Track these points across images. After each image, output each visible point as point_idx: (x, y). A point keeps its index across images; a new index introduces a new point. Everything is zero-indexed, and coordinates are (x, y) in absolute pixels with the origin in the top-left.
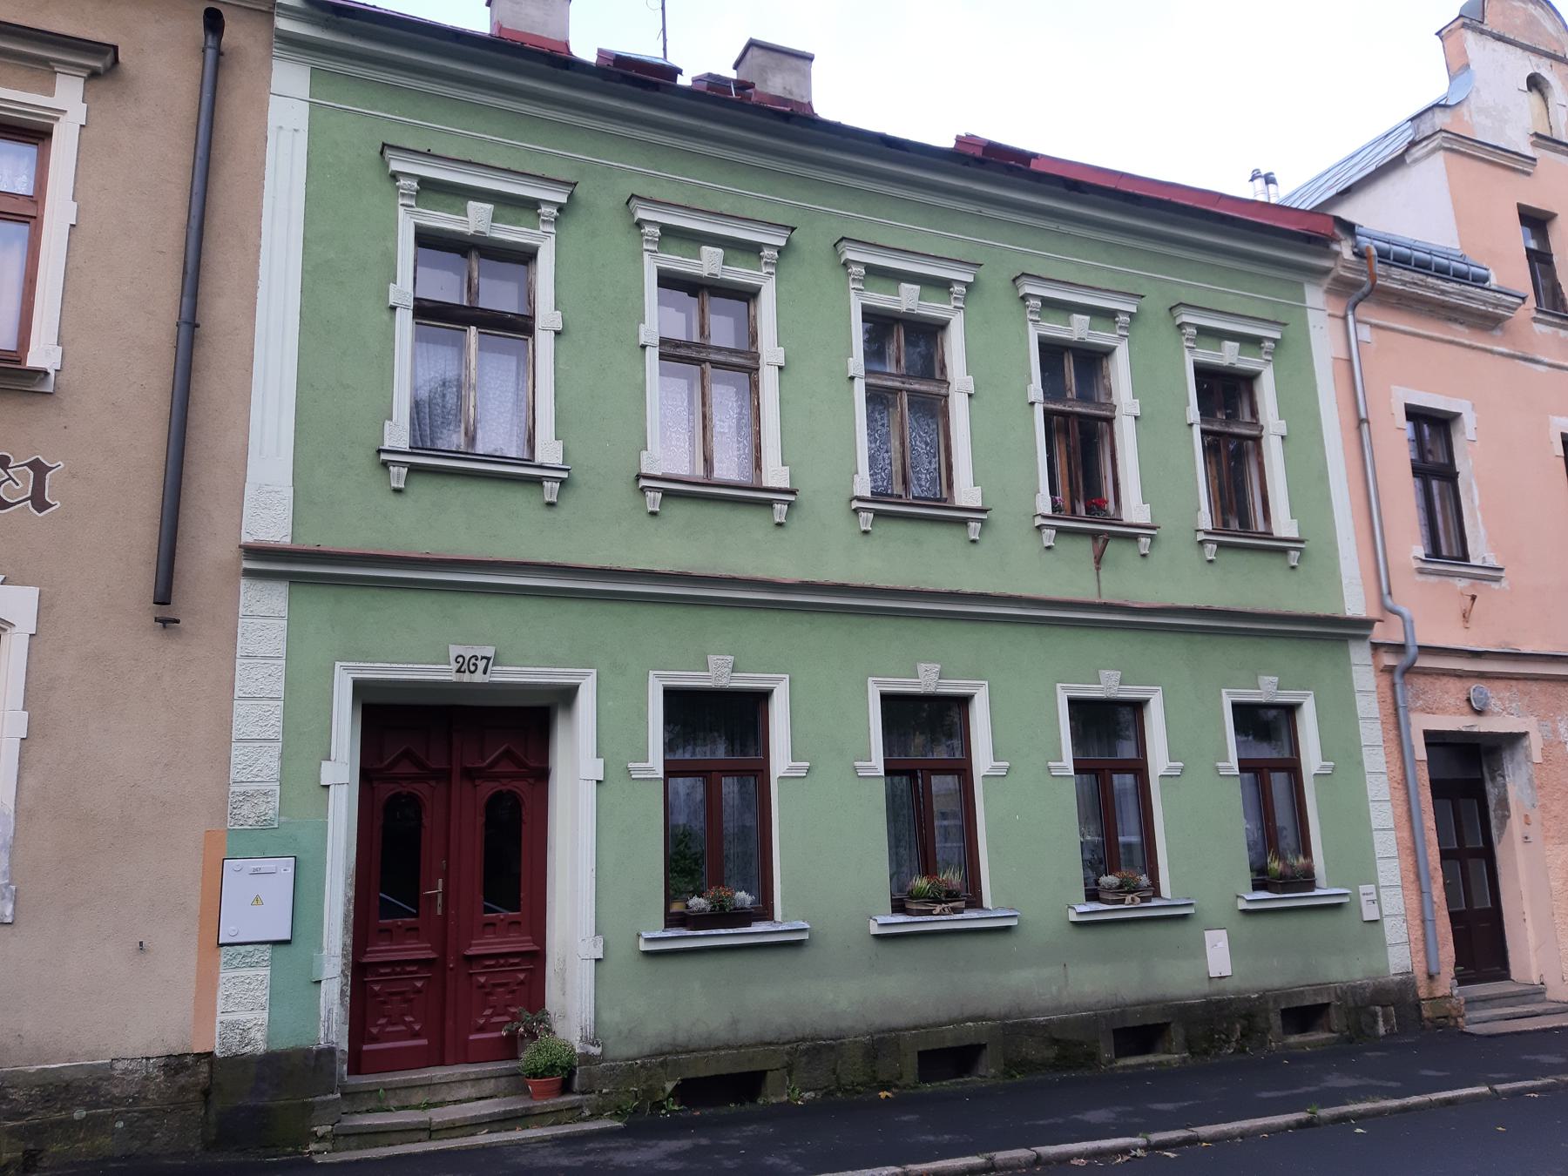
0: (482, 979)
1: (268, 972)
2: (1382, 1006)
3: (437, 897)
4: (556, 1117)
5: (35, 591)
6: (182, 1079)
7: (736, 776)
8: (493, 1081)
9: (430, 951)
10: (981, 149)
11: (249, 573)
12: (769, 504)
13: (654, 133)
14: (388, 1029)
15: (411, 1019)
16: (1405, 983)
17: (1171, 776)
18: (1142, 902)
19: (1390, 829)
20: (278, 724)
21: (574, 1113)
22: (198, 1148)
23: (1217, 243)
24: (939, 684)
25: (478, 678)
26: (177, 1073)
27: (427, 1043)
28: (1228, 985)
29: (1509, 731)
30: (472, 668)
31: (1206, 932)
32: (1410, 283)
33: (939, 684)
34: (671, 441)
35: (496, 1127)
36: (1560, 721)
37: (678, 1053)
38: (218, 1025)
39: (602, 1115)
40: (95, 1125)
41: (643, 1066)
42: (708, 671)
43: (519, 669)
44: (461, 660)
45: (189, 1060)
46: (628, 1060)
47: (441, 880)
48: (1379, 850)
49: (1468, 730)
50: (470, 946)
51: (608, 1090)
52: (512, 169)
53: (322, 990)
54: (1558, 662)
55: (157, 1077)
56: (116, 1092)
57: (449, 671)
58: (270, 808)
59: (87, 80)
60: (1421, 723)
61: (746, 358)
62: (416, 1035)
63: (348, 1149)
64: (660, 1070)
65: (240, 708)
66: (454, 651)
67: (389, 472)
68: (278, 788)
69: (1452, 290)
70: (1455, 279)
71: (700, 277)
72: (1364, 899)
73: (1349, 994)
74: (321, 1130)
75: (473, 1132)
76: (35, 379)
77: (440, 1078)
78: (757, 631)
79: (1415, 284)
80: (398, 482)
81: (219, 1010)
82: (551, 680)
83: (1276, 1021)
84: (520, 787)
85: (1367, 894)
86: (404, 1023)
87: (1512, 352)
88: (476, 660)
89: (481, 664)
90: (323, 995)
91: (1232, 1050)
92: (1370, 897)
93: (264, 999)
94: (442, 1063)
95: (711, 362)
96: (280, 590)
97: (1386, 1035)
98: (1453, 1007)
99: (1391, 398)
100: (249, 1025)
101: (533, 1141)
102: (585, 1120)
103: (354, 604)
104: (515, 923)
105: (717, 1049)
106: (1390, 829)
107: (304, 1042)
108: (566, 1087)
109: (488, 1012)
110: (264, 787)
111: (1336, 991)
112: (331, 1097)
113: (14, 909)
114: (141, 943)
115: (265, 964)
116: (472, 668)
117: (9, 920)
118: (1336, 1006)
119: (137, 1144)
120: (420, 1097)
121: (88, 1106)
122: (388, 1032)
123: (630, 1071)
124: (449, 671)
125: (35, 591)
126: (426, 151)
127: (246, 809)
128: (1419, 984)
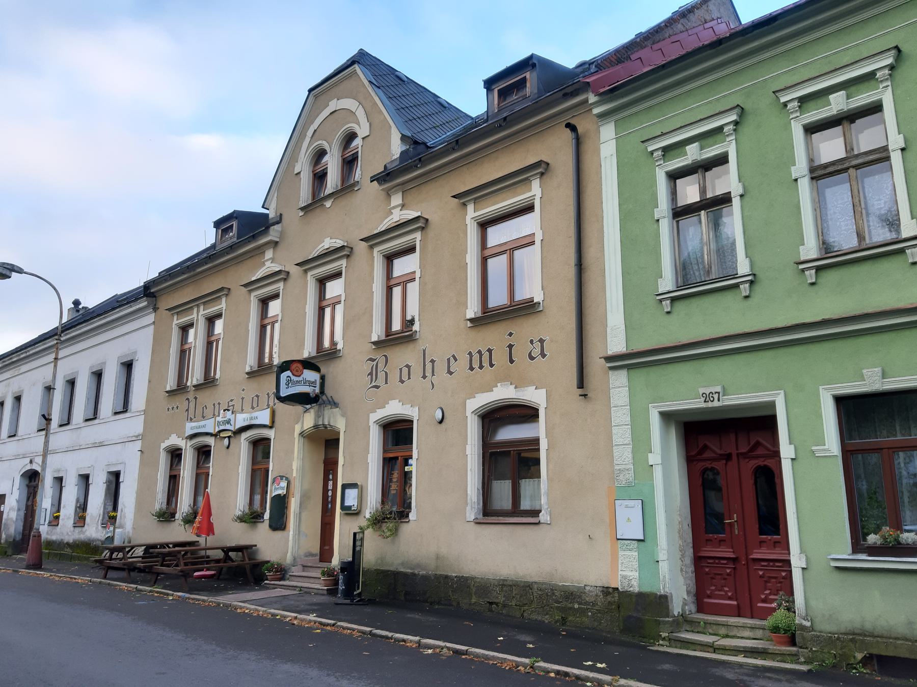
0: (707, 570)
1: (637, 554)
3: (734, 524)
4: (783, 657)
5: (544, 390)
6: (609, 598)
7: (876, 452)
8: (761, 631)
9: (732, 553)
11: (611, 368)
13: (643, 103)
14: (716, 593)
15: (727, 589)
20: (629, 436)
21: (794, 657)
22: (617, 631)
25: (716, 404)
26: (607, 595)
30: (712, 399)
34: (841, 228)
35: (748, 654)
37: (865, 636)
38: (619, 576)
39: (812, 663)
40: (582, 612)
41: (838, 639)
42: (865, 380)
43: (737, 396)
44: (704, 395)
45: (611, 590)
46: (830, 633)
47: (735, 515)
50: (753, 553)
51: (816, 649)
52: (682, 126)
53: (660, 566)
55: (600, 595)
56: (587, 599)
57: (700, 402)
58: (630, 476)
59: (540, 178)
61: (880, 153)
62: (730, 598)
63: (676, 647)
64: (851, 644)
65: (615, 430)
66: (701, 391)
67: (805, 274)
68: (632, 467)
71: (833, 116)
74: (664, 635)
75: (736, 654)
76: (535, 307)
77: (732, 623)
80: (667, 308)
81: (620, 569)
82: (757, 400)
84: (769, 463)
86: (724, 591)
88: (713, 394)
89: (716, 396)
90: (660, 568)
93: (636, 566)
94: (739, 615)
95: (853, 167)
96: (623, 373)
100: (631, 578)
101: (751, 665)
102: (801, 663)
103: (654, 374)
104: (721, 541)
105: (897, 639)
107: (654, 590)
108: (792, 642)
109: (767, 592)
110: (628, 467)
112: (667, 619)
113: (550, 518)
114: (589, 536)
115: (635, 550)
116: (712, 399)
117: (549, 523)
119: (596, 624)
120: (723, 631)
121: (580, 604)
122: (716, 594)
123: (831, 640)
124: (700, 402)
125: (544, 390)
126: (660, 134)
127: (621, 477)
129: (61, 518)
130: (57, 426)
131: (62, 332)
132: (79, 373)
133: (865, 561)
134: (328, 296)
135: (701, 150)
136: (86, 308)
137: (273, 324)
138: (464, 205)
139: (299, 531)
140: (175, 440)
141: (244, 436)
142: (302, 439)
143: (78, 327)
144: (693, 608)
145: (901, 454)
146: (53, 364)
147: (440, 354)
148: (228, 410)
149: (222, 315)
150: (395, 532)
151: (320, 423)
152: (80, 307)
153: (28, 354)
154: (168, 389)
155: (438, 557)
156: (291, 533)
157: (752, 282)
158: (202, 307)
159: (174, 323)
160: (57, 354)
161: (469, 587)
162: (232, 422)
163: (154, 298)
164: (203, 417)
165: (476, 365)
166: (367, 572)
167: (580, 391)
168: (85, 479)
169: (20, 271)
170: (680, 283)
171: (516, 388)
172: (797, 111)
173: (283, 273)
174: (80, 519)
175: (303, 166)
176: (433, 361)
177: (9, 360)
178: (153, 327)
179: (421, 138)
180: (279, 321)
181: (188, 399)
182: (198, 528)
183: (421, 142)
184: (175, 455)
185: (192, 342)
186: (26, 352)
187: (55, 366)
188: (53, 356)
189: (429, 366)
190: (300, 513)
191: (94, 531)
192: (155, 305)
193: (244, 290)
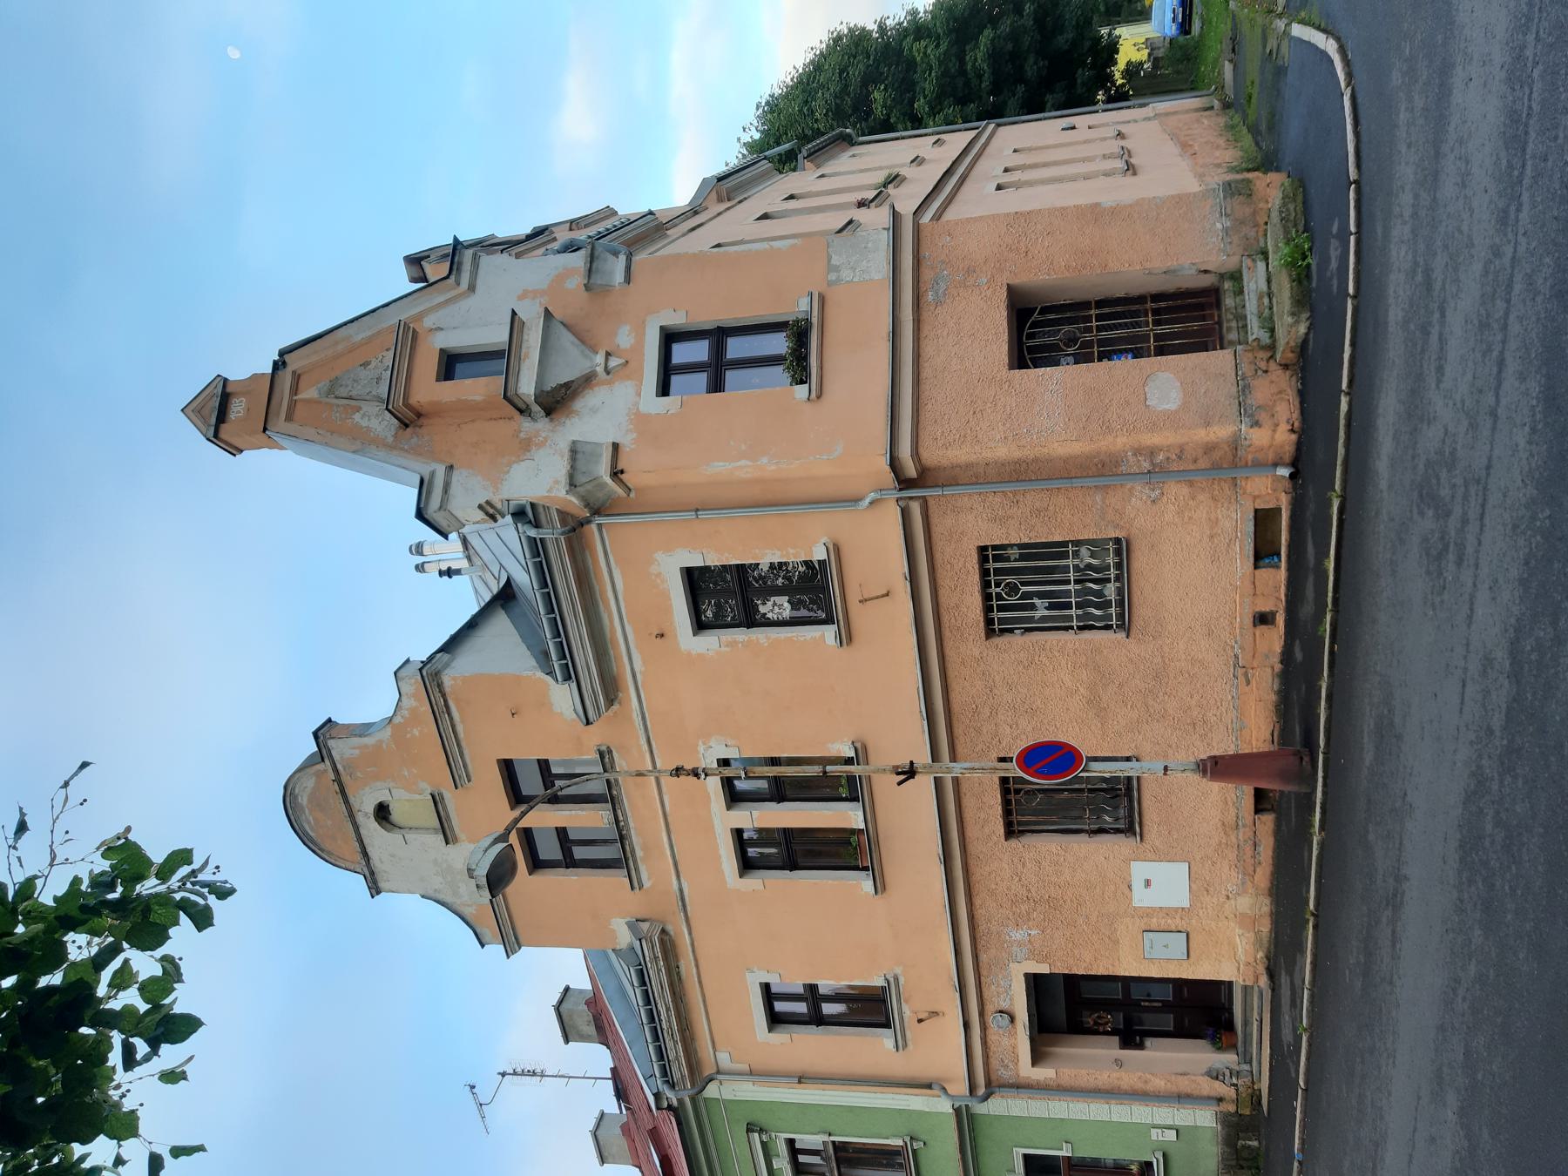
2: (1238, 1139)
27: (31, 1058)
32: (673, 1038)
60: (1026, 1069)
69: (664, 1006)
79: (672, 1035)
87: (684, 923)
92: (1160, 1135)
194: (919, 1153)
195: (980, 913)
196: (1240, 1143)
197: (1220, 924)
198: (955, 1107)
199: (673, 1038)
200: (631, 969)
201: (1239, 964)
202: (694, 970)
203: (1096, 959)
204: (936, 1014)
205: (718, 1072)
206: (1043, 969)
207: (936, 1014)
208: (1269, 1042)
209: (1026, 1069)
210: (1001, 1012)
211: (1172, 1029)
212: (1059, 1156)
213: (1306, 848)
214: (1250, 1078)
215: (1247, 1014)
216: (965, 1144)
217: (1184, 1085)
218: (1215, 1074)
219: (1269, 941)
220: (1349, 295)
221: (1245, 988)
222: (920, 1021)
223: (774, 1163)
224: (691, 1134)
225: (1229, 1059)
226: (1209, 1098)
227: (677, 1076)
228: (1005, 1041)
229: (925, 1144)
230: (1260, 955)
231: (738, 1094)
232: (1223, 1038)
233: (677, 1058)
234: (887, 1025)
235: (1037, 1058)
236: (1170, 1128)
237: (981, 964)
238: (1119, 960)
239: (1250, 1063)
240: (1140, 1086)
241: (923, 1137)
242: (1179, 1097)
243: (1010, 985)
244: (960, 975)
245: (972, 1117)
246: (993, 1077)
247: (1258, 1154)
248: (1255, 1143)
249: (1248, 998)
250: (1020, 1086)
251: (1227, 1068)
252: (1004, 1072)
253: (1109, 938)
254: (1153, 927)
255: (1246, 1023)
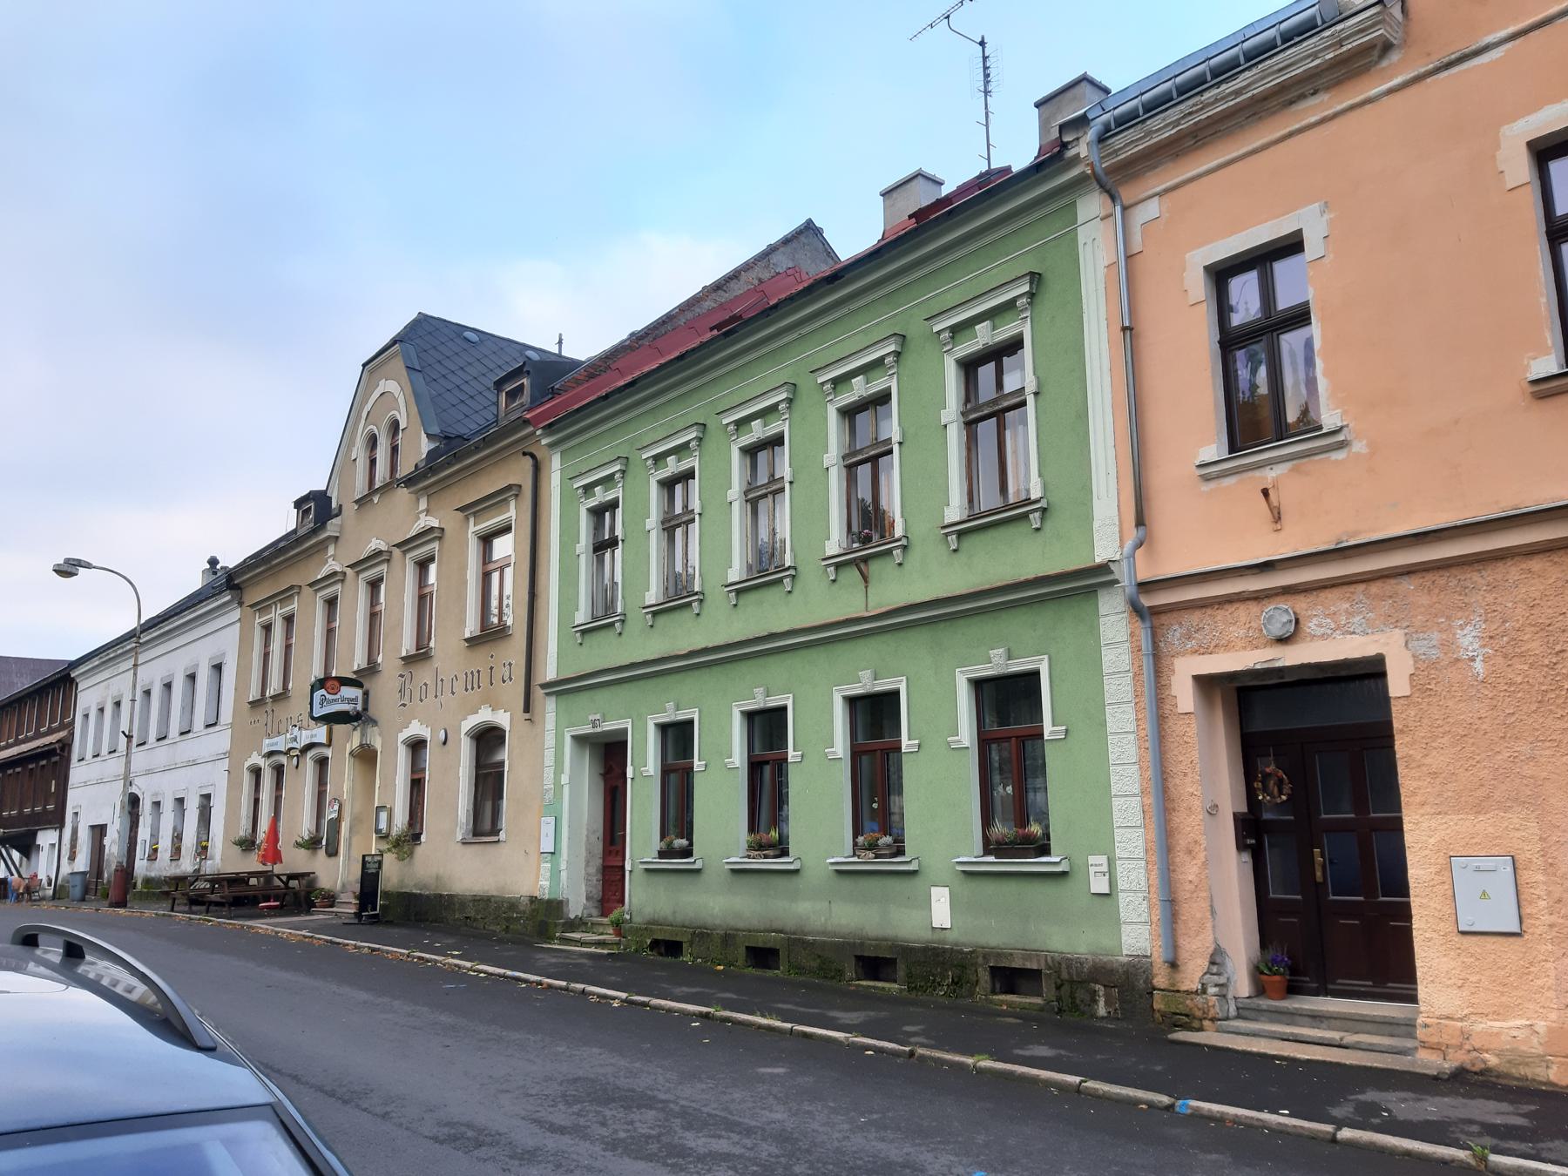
2: (1105, 986)
10: (1090, 118)
11: (547, 694)
12: (1025, 516)
16: (1134, 966)
17: (912, 752)
18: (876, 858)
19: (1134, 795)
23: (884, 275)
24: (765, 702)
28: (951, 937)
29: (1342, 657)
31: (933, 889)
32: (1183, 118)
33: (874, 685)
36: (1462, 627)
40: (518, 919)
48: (1118, 819)
49: (1265, 666)
54: (1440, 539)
60: (1185, 670)
66: (591, 718)
70: (1183, 98)
72: (1092, 870)
73: (1064, 965)
78: (1017, 625)
79: (1190, 114)
83: (984, 976)
85: (1096, 865)
91: (943, 993)
96: (553, 698)
97: (1106, 1017)
98: (1196, 1006)
99: (1184, 270)
106: (1134, 795)
111: (1046, 961)
118: (1046, 974)
128: (1155, 971)
129: (159, 851)
130: (155, 740)
131: (142, 632)
132: (200, 665)
133: (992, 863)
134: (496, 557)
135: (867, 384)
136: (226, 568)
137: (502, 569)
138: (467, 518)
139: (349, 857)
140: (256, 759)
141: (310, 754)
142: (352, 760)
143: (170, 620)
144: (595, 912)
145: (994, 746)
146: (132, 671)
147: (446, 676)
148: (296, 726)
149: (434, 558)
150: (411, 854)
151: (364, 742)
152: (218, 567)
153: (125, 649)
154: (467, 635)
155: (438, 878)
156: (341, 858)
157: (623, 621)
158: (472, 520)
159: (470, 531)
160: (136, 660)
161: (454, 904)
162: (298, 740)
163: (239, 591)
164: (279, 733)
165: (469, 687)
166: (386, 894)
167: (527, 716)
168: (180, 801)
169: (88, 566)
170: (671, 591)
171: (493, 710)
172: (1026, 308)
173: (339, 574)
174: (177, 852)
175: (359, 452)
176: (442, 680)
177: (106, 656)
178: (238, 624)
179: (453, 431)
180: (512, 564)
181: (266, 712)
182: (263, 856)
183: (453, 436)
184: (256, 772)
185: (433, 584)
186: (122, 648)
187: (135, 674)
188: (132, 662)
189: (439, 683)
190: (350, 838)
191: (187, 865)
192: (241, 599)
193: (311, 590)
194: (888, 559)
195: (1512, 572)
196: (1100, 988)
197: (1551, 994)
198: (1111, 564)
199: (1183, 118)
200: (1313, 9)
201: (1461, 1020)
202: (1313, 119)
203: (1435, 775)
204: (1277, 517)
205: (1125, 209)
206: (1398, 684)
207: (1277, 517)
208: (1320, 1058)
209: (1185, 670)
210: (1297, 621)
211: (1271, 895)
212: (693, 758)
213: (933, 1042)
214: (1220, 1016)
215: (1333, 1021)
216: (1043, 586)
217: (1194, 910)
218: (1218, 960)
219: (1525, 1079)
220: (1339, 1128)
221: (1407, 1027)
222: (1265, 493)
223: (757, 421)
224: (869, 272)
225: (1242, 986)
226: (1175, 947)
227: (1117, 142)
228: (1237, 632)
229: (790, 592)
230: (1492, 1060)
231: (1089, 248)
232: (1277, 978)
233: (1149, 133)
234: (1233, 448)
235: (1206, 684)
236: (1112, 883)
237: (1393, 581)
238: (1440, 813)
239: (1238, 1017)
240: (1182, 842)
241: (1048, 525)
242: (1173, 901)
243: (1354, 633)
244: (1369, 547)
245: (1091, 592)
246: (1164, 619)
247: (1083, 1013)
248: (1102, 1010)
249: (1369, 1027)
250: (1158, 663)
251: (1228, 979)
252: (1177, 634)
253: (1488, 797)
254: (1525, 876)
255: (1317, 1018)
